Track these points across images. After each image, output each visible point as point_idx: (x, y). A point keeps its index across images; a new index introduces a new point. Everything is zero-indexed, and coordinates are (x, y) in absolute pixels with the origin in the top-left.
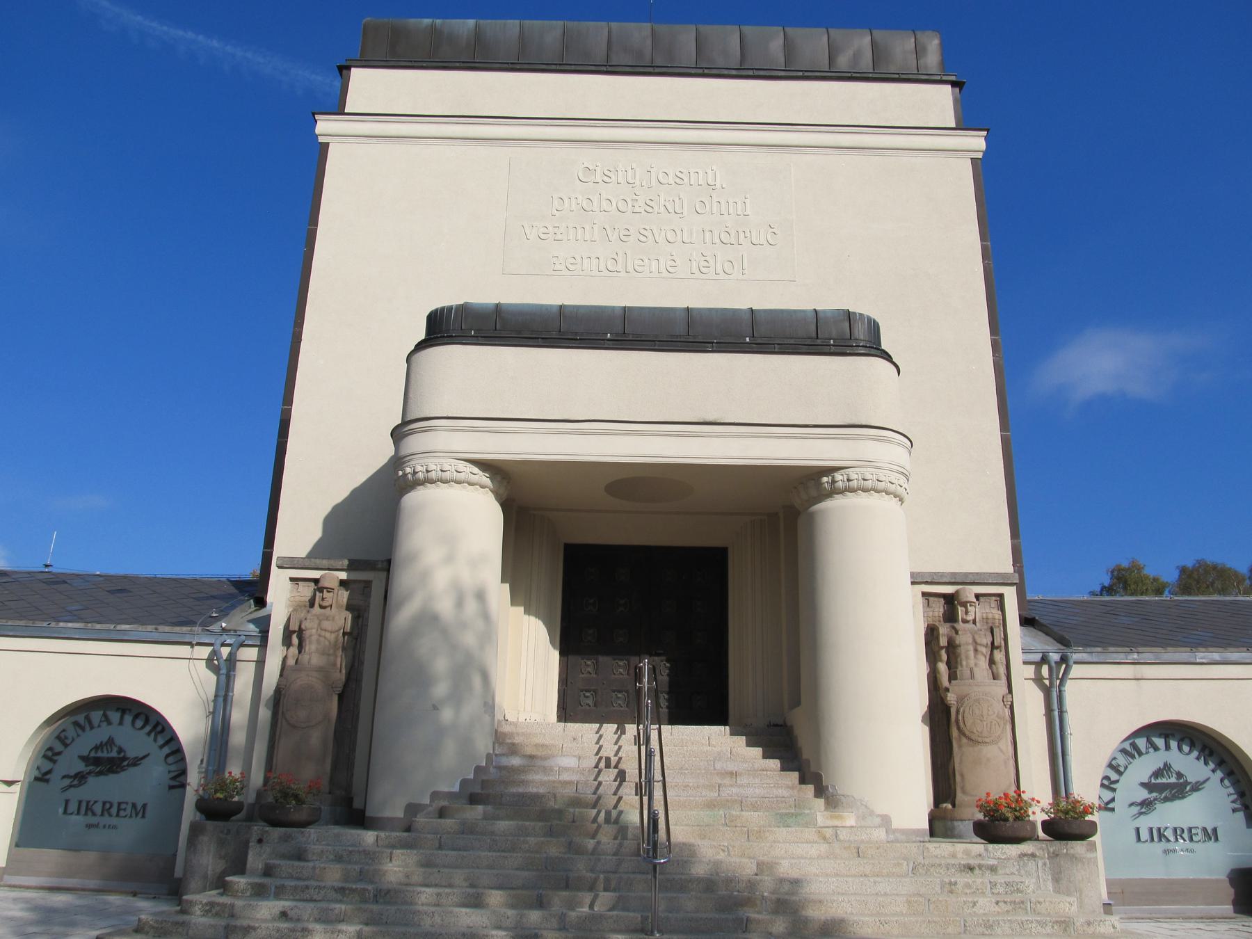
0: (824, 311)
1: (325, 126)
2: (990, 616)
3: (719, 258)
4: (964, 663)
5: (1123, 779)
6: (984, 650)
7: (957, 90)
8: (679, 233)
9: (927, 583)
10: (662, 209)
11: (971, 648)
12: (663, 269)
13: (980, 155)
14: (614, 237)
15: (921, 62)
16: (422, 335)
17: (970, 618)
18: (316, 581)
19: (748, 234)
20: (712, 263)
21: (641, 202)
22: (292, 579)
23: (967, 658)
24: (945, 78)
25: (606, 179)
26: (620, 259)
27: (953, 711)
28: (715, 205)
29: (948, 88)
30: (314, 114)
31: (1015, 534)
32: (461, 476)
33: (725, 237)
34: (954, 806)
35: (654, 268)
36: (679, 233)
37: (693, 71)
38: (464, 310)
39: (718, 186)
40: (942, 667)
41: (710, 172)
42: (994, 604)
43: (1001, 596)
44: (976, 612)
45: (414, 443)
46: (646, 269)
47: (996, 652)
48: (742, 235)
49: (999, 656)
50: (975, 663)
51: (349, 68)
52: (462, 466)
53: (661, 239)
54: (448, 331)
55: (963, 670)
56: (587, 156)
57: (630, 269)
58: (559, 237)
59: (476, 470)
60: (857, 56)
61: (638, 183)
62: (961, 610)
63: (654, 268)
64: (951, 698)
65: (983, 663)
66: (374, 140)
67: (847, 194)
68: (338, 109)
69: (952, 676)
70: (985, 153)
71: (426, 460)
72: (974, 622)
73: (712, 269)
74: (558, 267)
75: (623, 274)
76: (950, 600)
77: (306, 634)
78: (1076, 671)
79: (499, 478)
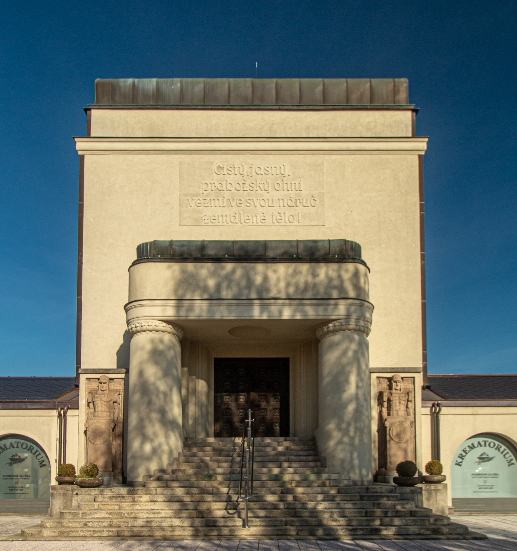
0: (333, 240)
1: (81, 145)
2: (408, 387)
3: (287, 214)
4: (394, 408)
5: (468, 455)
6: (403, 402)
7: (414, 114)
8: (267, 201)
9: (379, 372)
10: (258, 188)
11: (398, 401)
12: (259, 221)
13: (423, 153)
14: (234, 204)
15: (397, 98)
16: (135, 258)
17: (398, 388)
18: (99, 379)
19: (301, 201)
20: (283, 217)
21: (247, 185)
22: (87, 379)
23: (396, 406)
24: (408, 108)
25: (229, 172)
26: (237, 216)
27: (388, 429)
28: (285, 185)
29: (409, 114)
30: (74, 138)
31: (424, 348)
32: (158, 328)
33: (290, 203)
34: (386, 469)
35: (254, 221)
36: (267, 201)
37: (274, 107)
38: (154, 244)
39: (286, 175)
40: (385, 410)
41: (282, 167)
42: (410, 382)
43: (414, 378)
44: (401, 385)
45: (135, 312)
46: (251, 221)
47: (409, 402)
48: (298, 201)
49: (410, 405)
50: (399, 408)
51: (90, 110)
52: (158, 323)
54: (147, 256)
55: (394, 412)
56: (218, 160)
57: (242, 221)
58: (207, 205)
59: (164, 324)
60: (361, 97)
61: (245, 174)
62: (394, 384)
63: (254, 221)
64: (387, 424)
65: (403, 408)
66: (108, 153)
67: (331, 180)
68: (87, 134)
69: (389, 414)
70: (426, 152)
71: (141, 321)
72: (400, 390)
73: (283, 220)
74: (207, 221)
75: (239, 224)
76: (390, 379)
77: (96, 403)
78: (444, 410)
79: (180, 330)
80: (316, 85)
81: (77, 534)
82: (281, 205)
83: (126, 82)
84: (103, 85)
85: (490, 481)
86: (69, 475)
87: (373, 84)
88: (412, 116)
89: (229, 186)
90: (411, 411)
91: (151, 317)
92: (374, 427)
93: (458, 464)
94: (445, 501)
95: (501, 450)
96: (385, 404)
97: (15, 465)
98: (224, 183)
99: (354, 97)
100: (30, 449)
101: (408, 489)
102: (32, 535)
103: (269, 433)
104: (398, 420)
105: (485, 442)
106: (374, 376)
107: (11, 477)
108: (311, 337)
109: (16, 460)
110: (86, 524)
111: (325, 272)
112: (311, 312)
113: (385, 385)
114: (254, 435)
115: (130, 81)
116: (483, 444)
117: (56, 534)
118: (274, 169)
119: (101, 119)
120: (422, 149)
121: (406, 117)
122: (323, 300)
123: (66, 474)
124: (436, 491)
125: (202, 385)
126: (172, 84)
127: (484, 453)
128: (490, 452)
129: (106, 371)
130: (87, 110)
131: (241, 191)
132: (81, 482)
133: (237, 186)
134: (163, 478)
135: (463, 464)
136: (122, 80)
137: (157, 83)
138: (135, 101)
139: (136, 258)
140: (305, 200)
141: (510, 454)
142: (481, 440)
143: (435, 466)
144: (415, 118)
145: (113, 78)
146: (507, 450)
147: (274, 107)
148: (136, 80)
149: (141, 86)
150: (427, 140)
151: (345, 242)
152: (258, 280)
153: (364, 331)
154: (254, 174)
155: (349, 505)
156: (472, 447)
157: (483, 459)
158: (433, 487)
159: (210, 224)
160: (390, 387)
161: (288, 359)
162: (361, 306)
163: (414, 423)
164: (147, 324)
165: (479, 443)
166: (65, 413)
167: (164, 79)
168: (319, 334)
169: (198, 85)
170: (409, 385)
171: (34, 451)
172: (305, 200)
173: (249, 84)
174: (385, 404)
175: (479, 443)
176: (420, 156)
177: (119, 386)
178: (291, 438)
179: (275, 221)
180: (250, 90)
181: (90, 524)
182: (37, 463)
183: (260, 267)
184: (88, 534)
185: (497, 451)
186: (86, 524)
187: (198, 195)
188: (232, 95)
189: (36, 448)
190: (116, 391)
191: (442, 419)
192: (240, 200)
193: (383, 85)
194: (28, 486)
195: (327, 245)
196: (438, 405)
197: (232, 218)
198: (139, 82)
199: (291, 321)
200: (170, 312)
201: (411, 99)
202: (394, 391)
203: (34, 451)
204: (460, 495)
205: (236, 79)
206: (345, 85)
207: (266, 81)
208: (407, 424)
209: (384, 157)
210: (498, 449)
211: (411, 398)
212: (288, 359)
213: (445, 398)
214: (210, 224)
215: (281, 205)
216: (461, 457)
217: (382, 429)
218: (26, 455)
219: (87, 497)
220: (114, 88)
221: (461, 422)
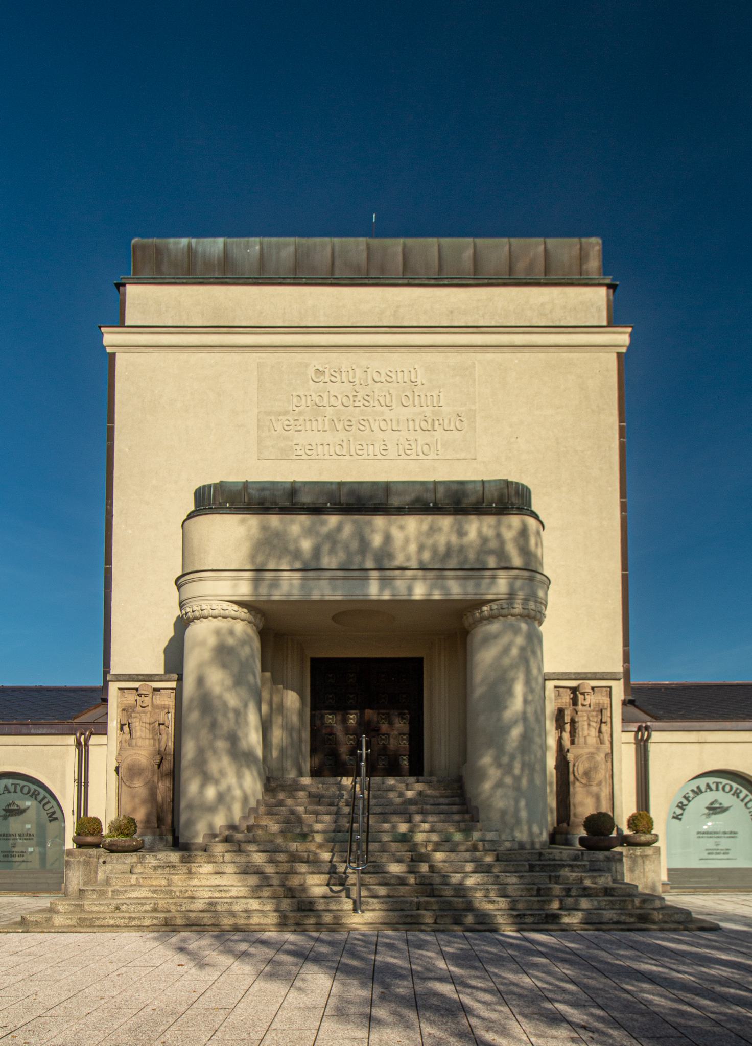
1: (111, 338)
3: (420, 442)
13: (624, 350)
15: (585, 267)
17: (587, 703)
18: (137, 689)
21: (359, 398)
26: (345, 445)
30: (100, 327)
33: (424, 424)
35: (371, 452)
40: (566, 736)
50: (588, 732)
51: (124, 285)
52: (226, 605)
53: (375, 428)
55: (580, 740)
56: (317, 360)
59: (236, 607)
62: (580, 697)
64: (570, 756)
69: (572, 742)
70: (629, 348)
73: (414, 451)
74: (299, 453)
78: (655, 736)
81: (105, 922)
82: (411, 428)
84: (144, 247)
85: (725, 843)
86: (92, 834)
87: (549, 246)
88: (608, 295)
89: (333, 399)
90: (606, 738)
91: (217, 597)
92: (551, 762)
93: (677, 817)
95: (742, 796)
97: (11, 819)
98: (325, 396)
99: (521, 266)
100: (34, 795)
101: (601, 855)
102: (37, 923)
103: (393, 770)
104: (587, 750)
105: (717, 784)
106: (550, 685)
108: (455, 627)
110: (117, 908)
112: (456, 589)
113: (567, 698)
114: (371, 772)
115: (184, 241)
116: (714, 787)
118: (400, 374)
119: (141, 299)
120: (622, 343)
122: (474, 570)
123: (88, 831)
124: (644, 857)
125: (292, 699)
126: (247, 246)
127: (716, 801)
128: (725, 799)
129: (149, 678)
130: (120, 286)
131: (351, 408)
132: (111, 845)
133: (345, 400)
134: (234, 839)
135: (683, 817)
136: (172, 240)
137: (225, 244)
138: (192, 272)
139: (193, 508)
140: (446, 421)
142: (711, 780)
143: (641, 820)
144: (611, 297)
145: (158, 237)
147: (400, 282)
148: (194, 241)
149: (200, 249)
150: (630, 330)
152: (377, 540)
154: (370, 381)
155: (513, 879)
156: (698, 792)
157: (714, 809)
158: (638, 851)
159: (305, 457)
160: (575, 702)
164: (209, 607)
165: (708, 786)
171: (40, 797)
172: (446, 421)
173: (363, 247)
175: (708, 786)
176: (619, 355)
177: (168, 700)
179: (401, 452)
180: (365, 256)
181: (124, 908)
182: (44, 815)
183: (379, 521)
185: (735, 797)
186: (117, 908)
187: (286, 413)
188: (337, 263)
190: (163, 707)
192: (350, 421)
193: (564, 248)
194: (31, 849)
195: (479, 488)
197: (338, 448)
198: (197, 243)
199: (427, 603)
200: (244, 590)
201: (606, 269)
202: (580, 707)
203: (40, 797)
204: (679, 864)
205: (344, 239)
208: (600, 757)
210: (737, 794)
211: (606, 718)
213: (657, 718)
214: (305, 457)
215: (411, 428)
216: (681, 806)
217: (563, 765)
218: (28, 803)
220: (159, 252)
221: (682, 755)
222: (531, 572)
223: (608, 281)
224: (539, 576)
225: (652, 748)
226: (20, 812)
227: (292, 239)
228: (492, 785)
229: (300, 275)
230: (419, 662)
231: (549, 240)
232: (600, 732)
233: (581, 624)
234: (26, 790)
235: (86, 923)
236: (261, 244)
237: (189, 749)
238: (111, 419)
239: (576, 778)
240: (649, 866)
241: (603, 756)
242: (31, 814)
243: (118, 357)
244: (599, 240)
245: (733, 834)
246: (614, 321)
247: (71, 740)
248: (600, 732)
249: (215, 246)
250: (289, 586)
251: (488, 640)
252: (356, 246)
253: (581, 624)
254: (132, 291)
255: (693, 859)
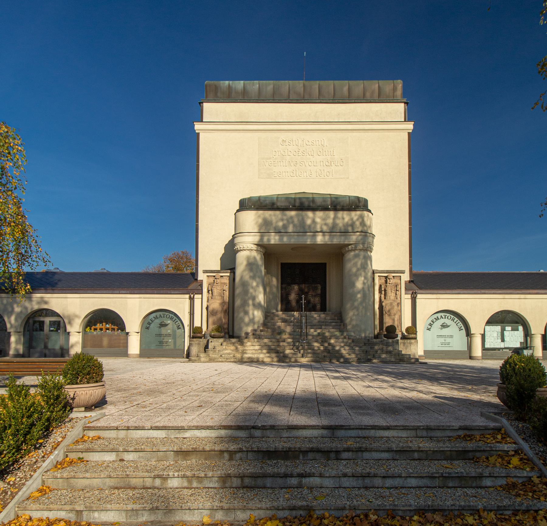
1: (198, 126)
3: (325, 171)
13: (411, 131)
15: (395, 93)
17: (391, 283)
18: (214, 276)
21: (300, 152)
26: (294, 172)
29: (402, 105)
33: (327, 163)
35: (305, 175)
38: (250, 199)
40: (383, 296)
50: (391, 295)
51: (202, 103)
53: (307, 165)
55: (388, 297)
56: (283, 136)
62: (388, 280)
64: (384, 304)
69: (385, 298)
70: (413, 130)
78: (419, 296)
80: (344, 86)
81: (218, 360)
82: (322, 165)
83: (225, 83)
85: (448, 340)
86: (199, 333)
87: (380, 84)
88: (405, 107)
89: (289, 153)
90: (398, 297)
91: (249, 243)
92: (377, 306)
93: (429, 329)
94: (416, 349)
95: (455, 321)
96: (383, 292)
97: (162, 328)
98: (286, 151)
99: (368, 94)
100: (171, 319)
101: (390, 340)
102: (195, 360)
103: (314, 309)
104: (390, 302)
106: (377, 275)
107: (160, 335)
108: (338, 253)
109: (163, 325)
110: (221, 356)
111: (345, 217)
112: (336, 241)
113: (383, 280)
115: (227, 82)
116: (444, 317)
117: (208, 360)
118: (317, 142)
119: (210, 109)
121: (400, 108)
122: (345, 232)
123: (196, 333)
124: (411, 343)
125: (274, 281)
126: (253, 84)
127: (444, 323)
128: (448, 322)
129: (218, 272)
130: (201, 103)
131: (297, 156)
132: (214, 335)
133: (294, 153)
134: (256, 335)
135: (431, 329)
136: (222, 82)
137: (244, 84)
138: (230, 97)
139: (238, 208)
140: (336, 162)
141: (461, 323)
142: (443, 314)
143: (412, 330)
146: (459, 321)
147: (317, 101)
148: (231, 82)
149: (234, 86)
151: (358, 198)
152: (309, 222)
153: (368, 248)
154: (305, 144)
155: (357, 348)
156: (437, 319)
157: (444, 326)
158: (409, 341)
159: (278, 177)
160: (386, 282)
161: (325, 264)
162: (366, 236)
163: (399, 304)
165: (441, 316)
166: (194, 296)
167: (248, 82)
168: (343, 251)
169: (269, 85)
170: (397, 281)
171: (173, 320)
172: (336, 162)
173: (302, 85)
174: (383, 292)
175: (441, 316)
177: (226, 281)
178: (327, 312)
179: (318, 175)
180: (302, 89)
181: (223, 356)
182: (175, 327)
183: (310, 214)
184: (224, 360)
186: (221, 356)
187: (270, 158)
188: (291, 92)
189: (175, 318)
190: (225, 284)
191: (418, 301)
193: (387, 86)
194: (170, 341)
195: (348, 199)
196: (415, 293)
197: (291, 174)
198: (232, 84)
201: (404, 95)
202: (388, 284)
203: (173, 320)
204: (430, 348)
205: (294, 81)
206: (362, 85)
207: (312, 82)
208: (395, 304)
209: (387, 133)
210: (453, 320)
211: (398, 288)
212: (325, 264)
213: (420, 288)
215: (322, 165)
216: (430, 325)
217: (381, 308)
218: (169, 322)
219: (217, 343)
220: (216, 88)
221: (430, 303)
222: (366, 235)
223: (405, 100)
224: (368, 234)
225: (417, 301)
226: (166, 325)
227: (272, 81)
228: (351, 316)
229: (275, 98)
230: (324, 265)
231: (380, 81)
232: (396, 294)
233: (389, 248)
234: (168, 316)
235: (211, 360)
236: (259, 84)
237: (238, 302)
238: (198, 161)
239: (386, 313)
240: (413, 347)
241: (396, 303)
242: (170, 326)
243: (200, 134)
244: (402, 82)
245: (451, 336)
246: (408, 119)
247: (187, 296)
248: (396, 294)
249: (239, 85)
250: (274, 239)
251: (350, 260)
252: (299, 85)
253: (389, 248)
254: (206, 105)
255: (436, 346)
